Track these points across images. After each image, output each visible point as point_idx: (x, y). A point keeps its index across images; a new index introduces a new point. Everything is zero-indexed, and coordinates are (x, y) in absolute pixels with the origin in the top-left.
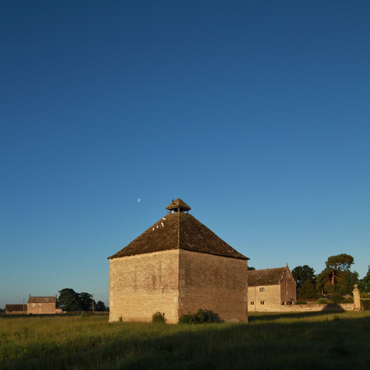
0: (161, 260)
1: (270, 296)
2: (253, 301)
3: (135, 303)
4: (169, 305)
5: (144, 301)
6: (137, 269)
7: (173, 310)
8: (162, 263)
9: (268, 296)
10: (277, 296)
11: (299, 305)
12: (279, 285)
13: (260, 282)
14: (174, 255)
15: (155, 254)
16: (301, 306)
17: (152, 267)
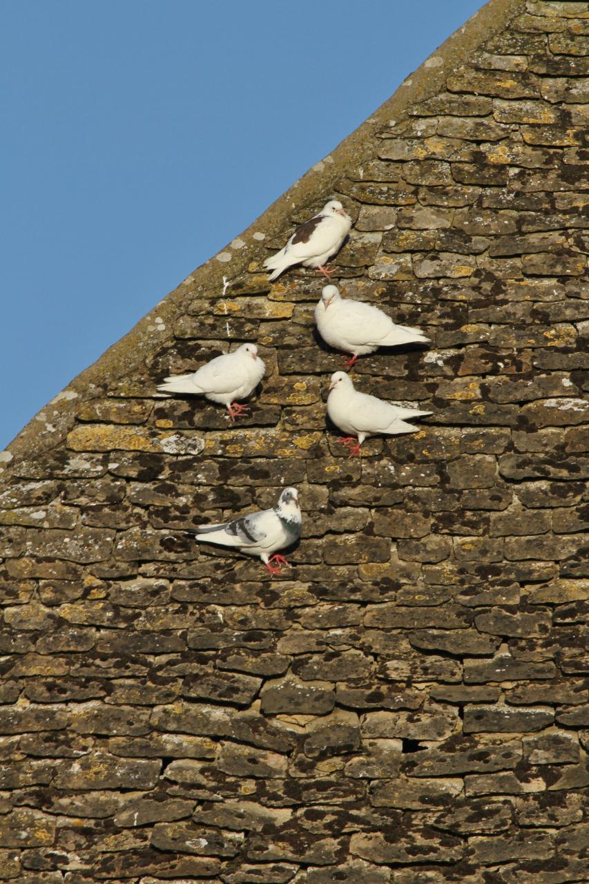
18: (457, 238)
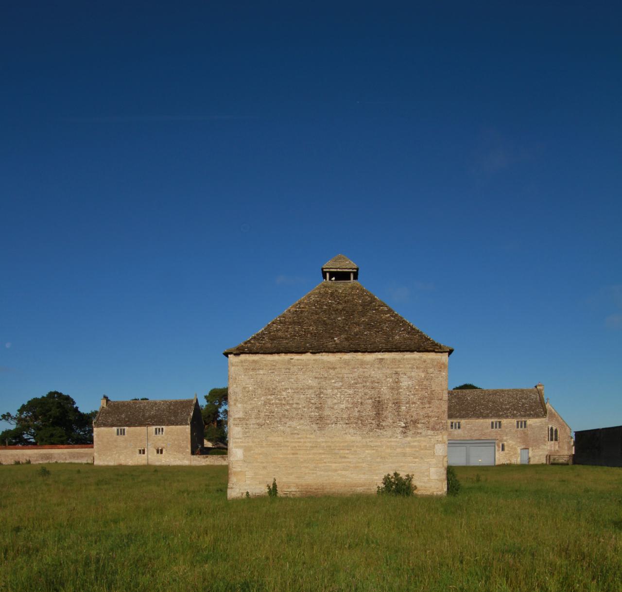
0: (398, 370)
1: (173, 442)
2: (143, 449)
3: (320, 453)
4: (422, 458)
5: (348, 450)
6: (324, 383)
7: (432, 470)
8: (402, 375)
9: (170, 441)
10: (185, 442)
11: (219, 456)
12: (187, 426)
13: (155, 420)
14: (435, 363)
15: (421, 355)
16: (223, 457)
17: (373, 382)
18: (318, 297)
